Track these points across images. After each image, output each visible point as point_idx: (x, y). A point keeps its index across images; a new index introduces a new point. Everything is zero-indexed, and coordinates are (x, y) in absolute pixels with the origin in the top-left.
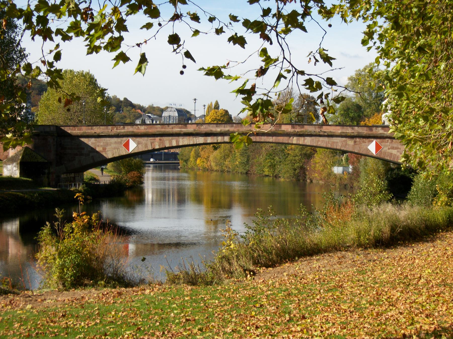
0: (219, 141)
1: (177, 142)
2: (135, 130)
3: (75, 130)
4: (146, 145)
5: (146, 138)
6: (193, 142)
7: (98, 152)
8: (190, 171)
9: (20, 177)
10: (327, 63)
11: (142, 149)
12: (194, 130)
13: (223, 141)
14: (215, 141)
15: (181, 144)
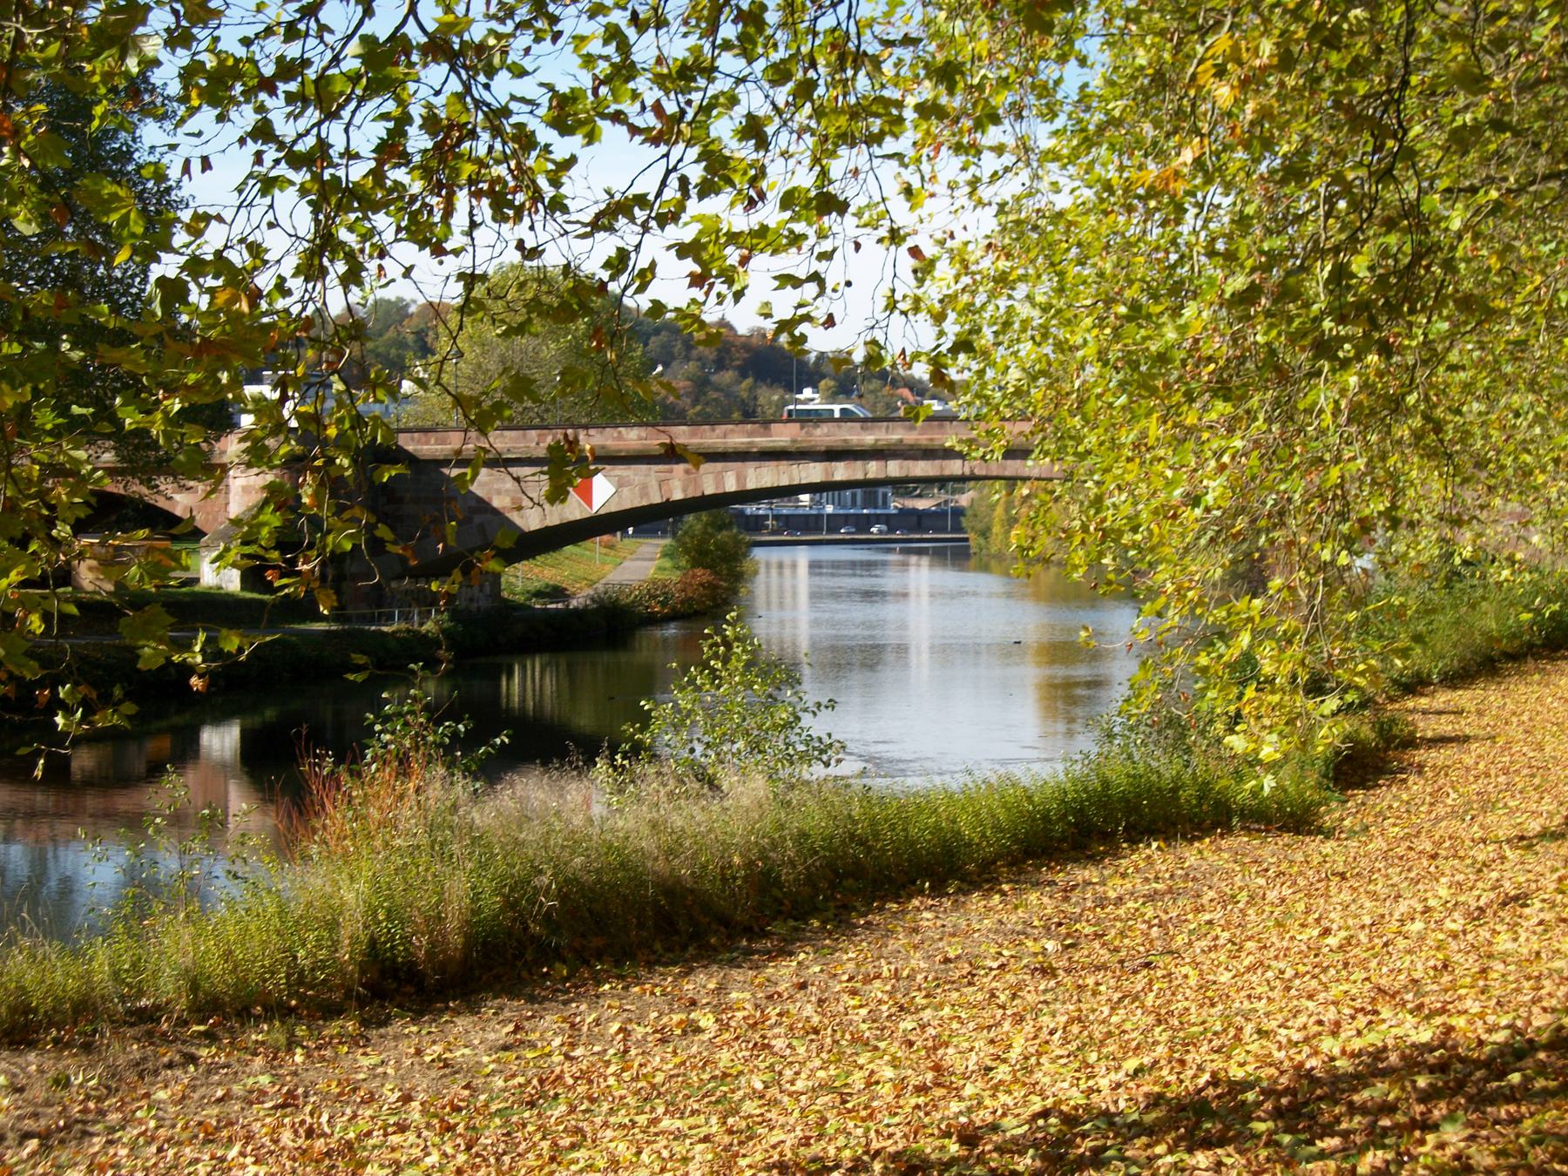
0: (871, 476)
1: (740, 478)
2: (609, 443)
3: (427, 443)
4: (644, 490)
5: (644, 467)
6: (791, 478)
7: (495, 512)
8: (993, 563)
9: (243, 589)
10: (567, 91)
11: (630, 500)
12: (794, 441)
13: (882, 476)
14: (859, 476)
15: (751, 485)
